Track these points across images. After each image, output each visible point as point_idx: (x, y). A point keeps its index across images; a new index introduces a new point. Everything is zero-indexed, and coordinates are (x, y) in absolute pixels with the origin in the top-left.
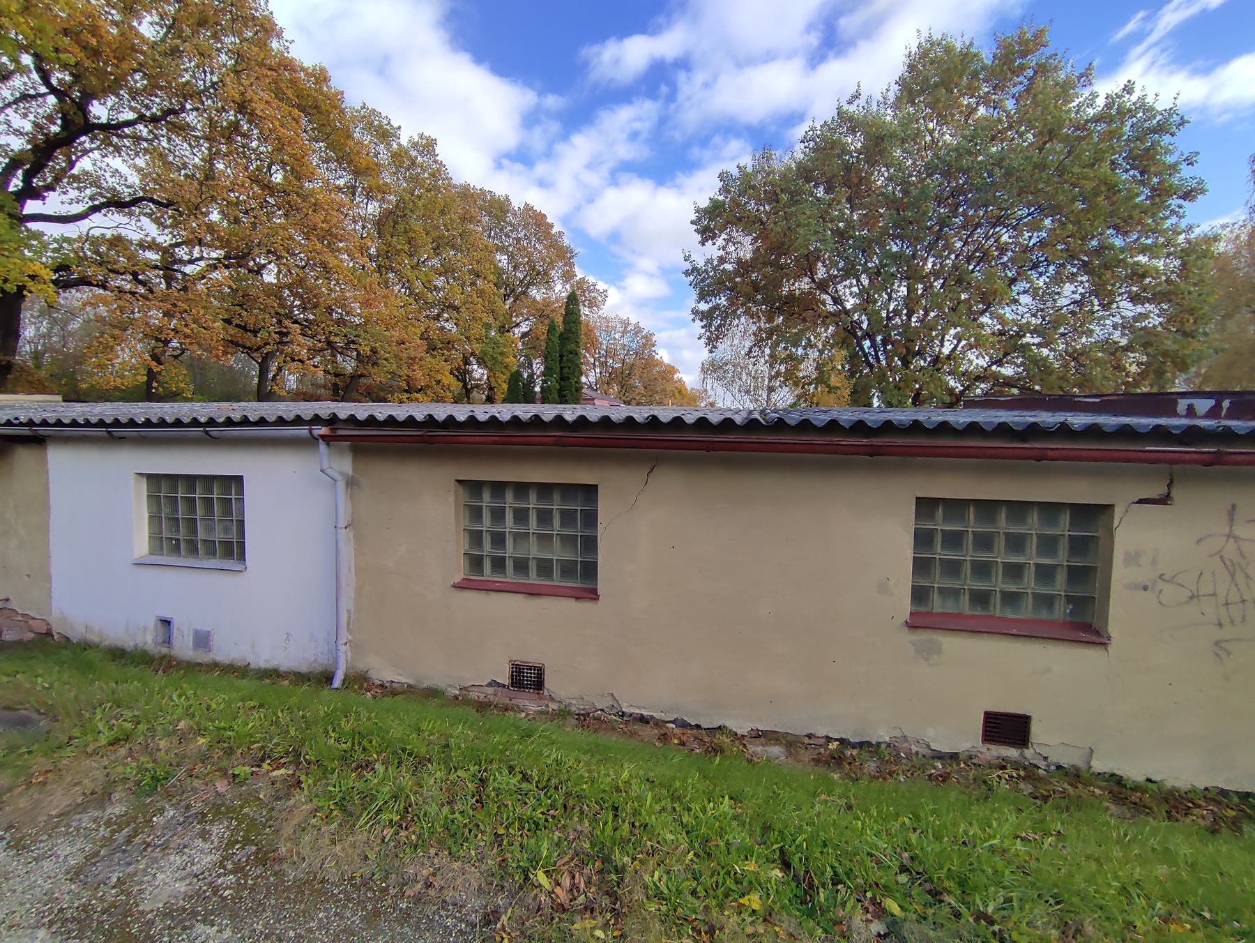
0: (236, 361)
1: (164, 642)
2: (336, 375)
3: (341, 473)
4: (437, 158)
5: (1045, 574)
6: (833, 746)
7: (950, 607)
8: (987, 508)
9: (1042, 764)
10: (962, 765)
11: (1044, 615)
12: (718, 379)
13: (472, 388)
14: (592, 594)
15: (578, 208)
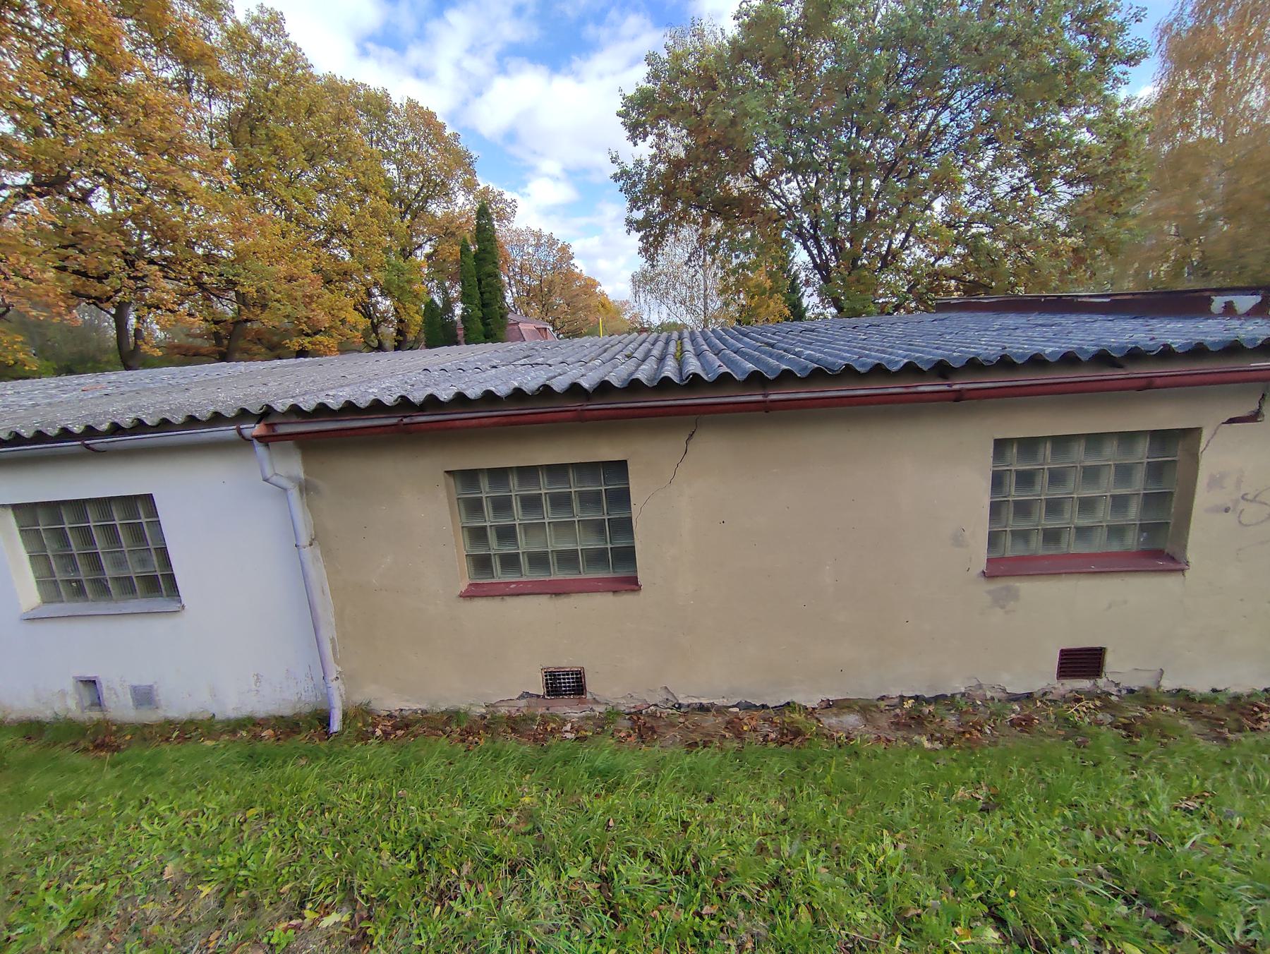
0: (82, 314)
1: (92, 705)
2: (216, 323)
3: (290, 478)
4: (290, 39)
5: (1120, 503)
6: (908, 704)
7: (1020, 550)
8: (1061, 442)
9: (1113, 690)
10: (1039, 704)
11: (1115, 547)
12: (651, 291)
13: (379, 322)
14: (631, 584)
15: (465, 103)
